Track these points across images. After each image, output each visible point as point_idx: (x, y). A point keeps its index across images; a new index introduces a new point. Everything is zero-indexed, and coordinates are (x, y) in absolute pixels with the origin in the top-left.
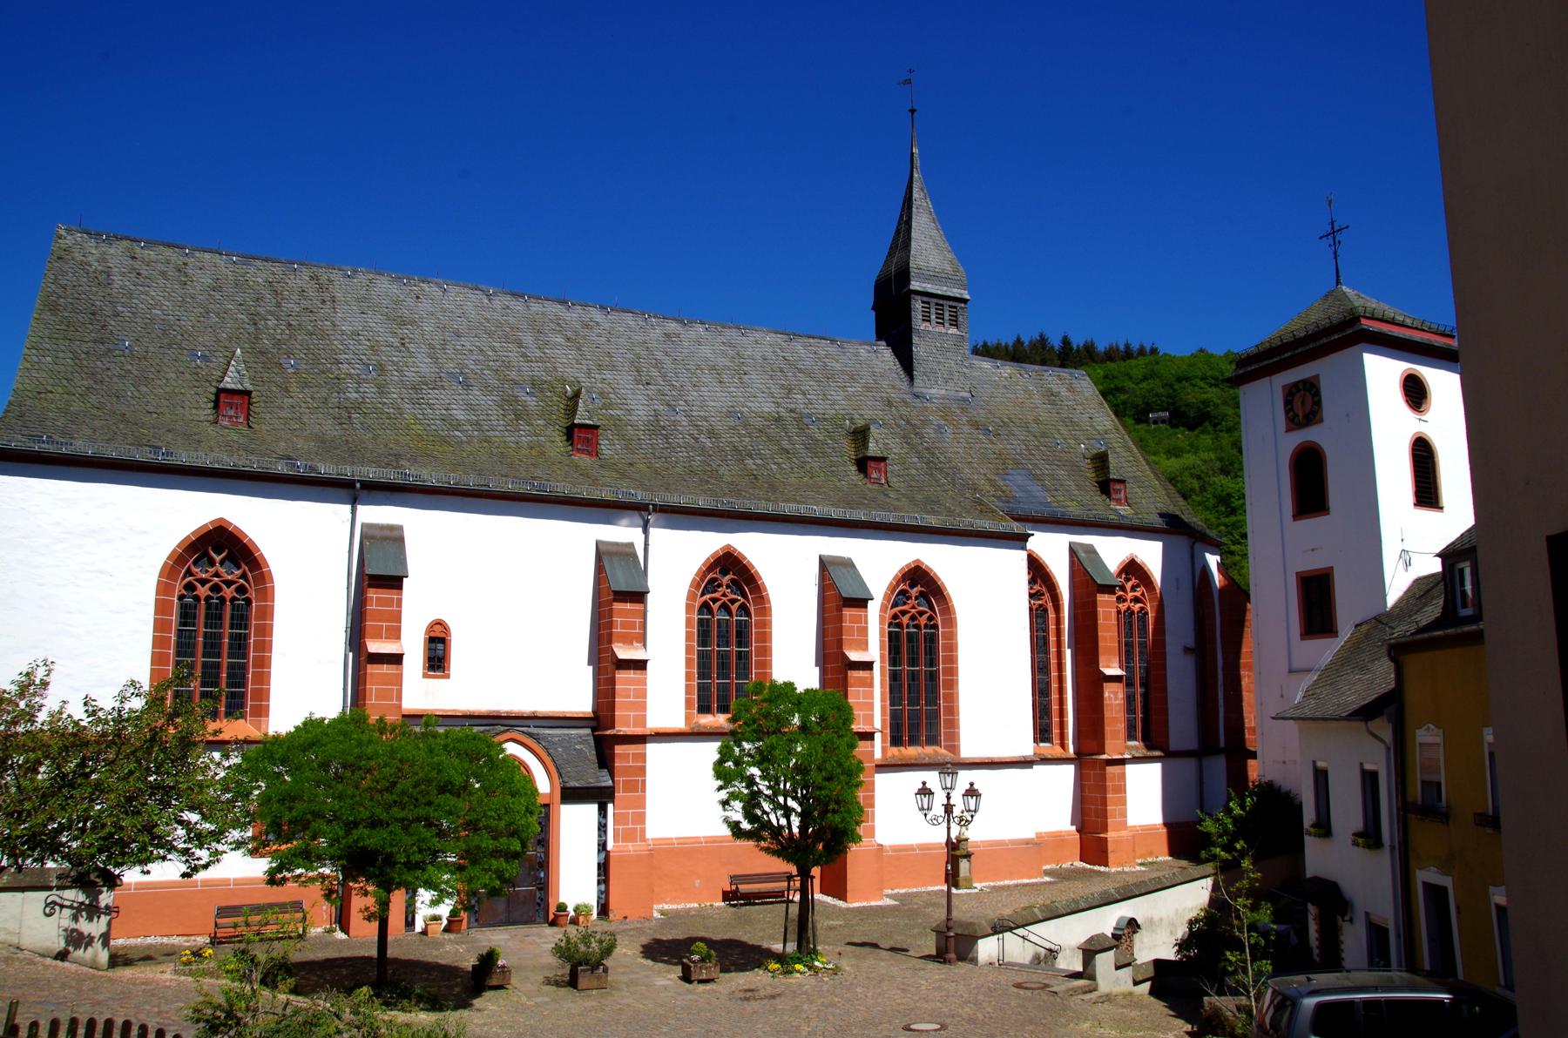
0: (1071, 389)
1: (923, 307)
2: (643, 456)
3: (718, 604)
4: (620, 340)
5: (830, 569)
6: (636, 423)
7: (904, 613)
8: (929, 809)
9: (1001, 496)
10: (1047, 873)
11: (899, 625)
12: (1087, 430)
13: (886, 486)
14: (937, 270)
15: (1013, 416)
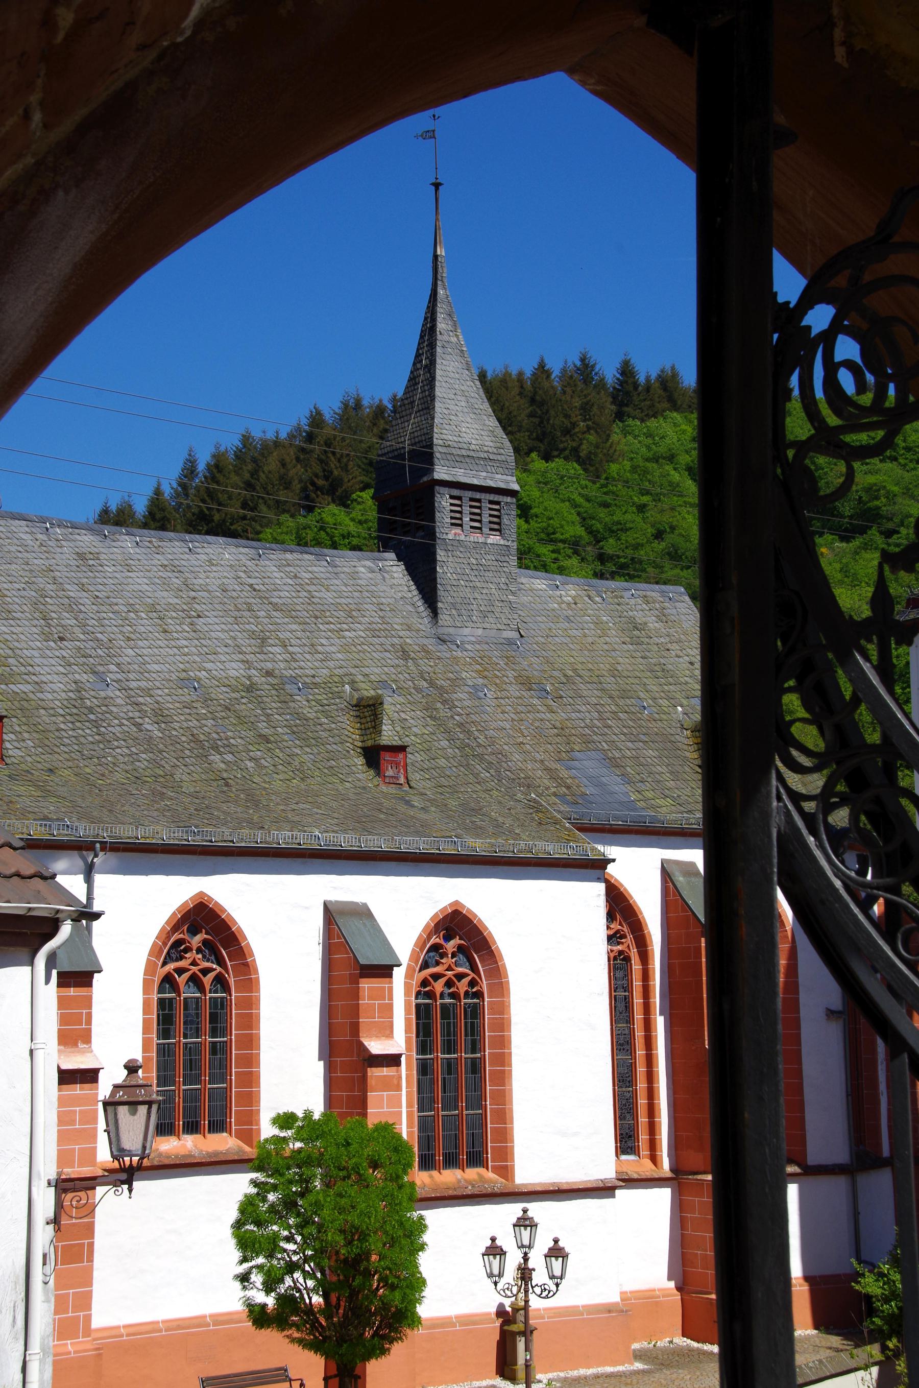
0: (663, 617)
1: (452, 505)
2: (66, 756)
3: (186, 976)
4: (13, 567)
5: (340, 921)
6: (52, 705)
7: (436, 977)
8: (500, 1275)
9: (565, 795)
10: (639, 1356)
11: (430, 995)
12: (686, 684)
13: (406, 788)
14: (471, 448)
15: (579, 666)
